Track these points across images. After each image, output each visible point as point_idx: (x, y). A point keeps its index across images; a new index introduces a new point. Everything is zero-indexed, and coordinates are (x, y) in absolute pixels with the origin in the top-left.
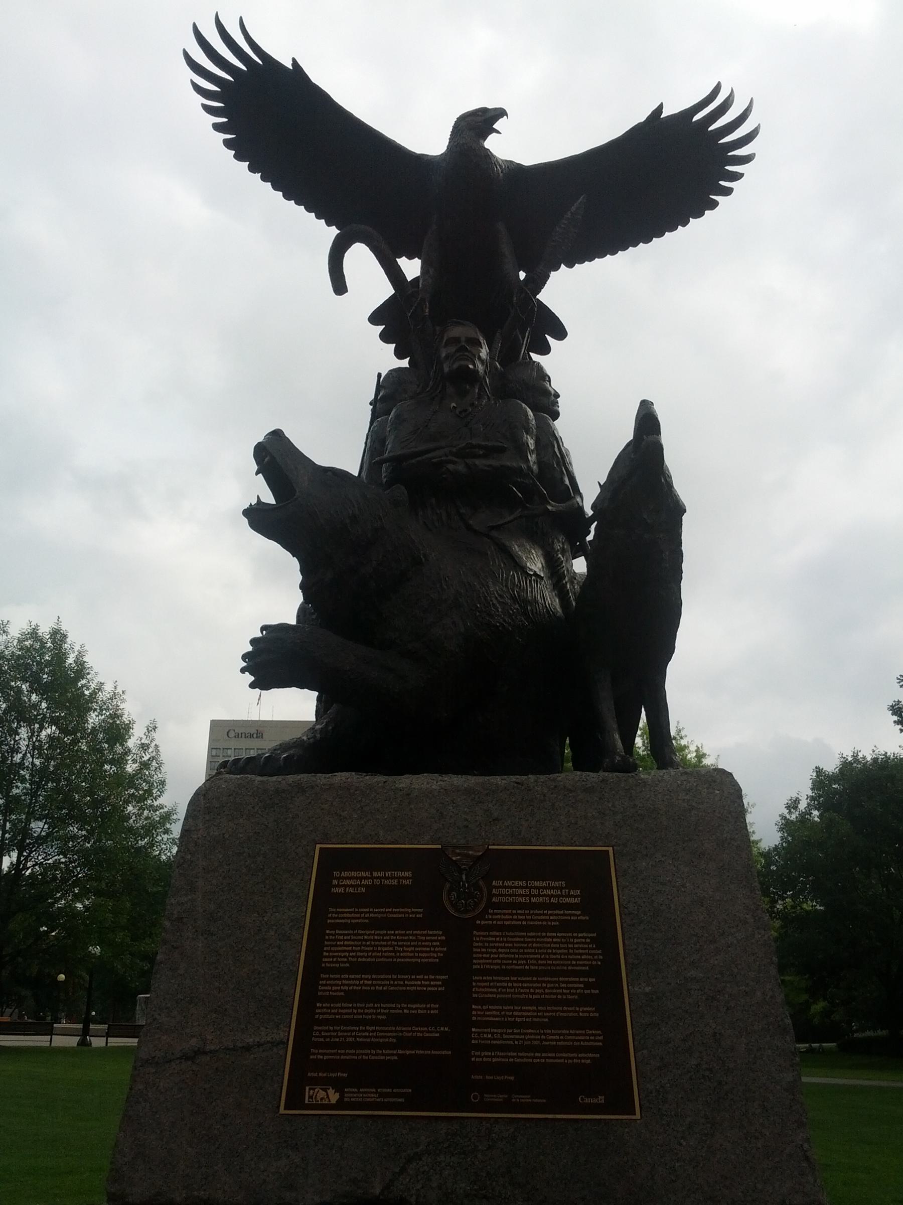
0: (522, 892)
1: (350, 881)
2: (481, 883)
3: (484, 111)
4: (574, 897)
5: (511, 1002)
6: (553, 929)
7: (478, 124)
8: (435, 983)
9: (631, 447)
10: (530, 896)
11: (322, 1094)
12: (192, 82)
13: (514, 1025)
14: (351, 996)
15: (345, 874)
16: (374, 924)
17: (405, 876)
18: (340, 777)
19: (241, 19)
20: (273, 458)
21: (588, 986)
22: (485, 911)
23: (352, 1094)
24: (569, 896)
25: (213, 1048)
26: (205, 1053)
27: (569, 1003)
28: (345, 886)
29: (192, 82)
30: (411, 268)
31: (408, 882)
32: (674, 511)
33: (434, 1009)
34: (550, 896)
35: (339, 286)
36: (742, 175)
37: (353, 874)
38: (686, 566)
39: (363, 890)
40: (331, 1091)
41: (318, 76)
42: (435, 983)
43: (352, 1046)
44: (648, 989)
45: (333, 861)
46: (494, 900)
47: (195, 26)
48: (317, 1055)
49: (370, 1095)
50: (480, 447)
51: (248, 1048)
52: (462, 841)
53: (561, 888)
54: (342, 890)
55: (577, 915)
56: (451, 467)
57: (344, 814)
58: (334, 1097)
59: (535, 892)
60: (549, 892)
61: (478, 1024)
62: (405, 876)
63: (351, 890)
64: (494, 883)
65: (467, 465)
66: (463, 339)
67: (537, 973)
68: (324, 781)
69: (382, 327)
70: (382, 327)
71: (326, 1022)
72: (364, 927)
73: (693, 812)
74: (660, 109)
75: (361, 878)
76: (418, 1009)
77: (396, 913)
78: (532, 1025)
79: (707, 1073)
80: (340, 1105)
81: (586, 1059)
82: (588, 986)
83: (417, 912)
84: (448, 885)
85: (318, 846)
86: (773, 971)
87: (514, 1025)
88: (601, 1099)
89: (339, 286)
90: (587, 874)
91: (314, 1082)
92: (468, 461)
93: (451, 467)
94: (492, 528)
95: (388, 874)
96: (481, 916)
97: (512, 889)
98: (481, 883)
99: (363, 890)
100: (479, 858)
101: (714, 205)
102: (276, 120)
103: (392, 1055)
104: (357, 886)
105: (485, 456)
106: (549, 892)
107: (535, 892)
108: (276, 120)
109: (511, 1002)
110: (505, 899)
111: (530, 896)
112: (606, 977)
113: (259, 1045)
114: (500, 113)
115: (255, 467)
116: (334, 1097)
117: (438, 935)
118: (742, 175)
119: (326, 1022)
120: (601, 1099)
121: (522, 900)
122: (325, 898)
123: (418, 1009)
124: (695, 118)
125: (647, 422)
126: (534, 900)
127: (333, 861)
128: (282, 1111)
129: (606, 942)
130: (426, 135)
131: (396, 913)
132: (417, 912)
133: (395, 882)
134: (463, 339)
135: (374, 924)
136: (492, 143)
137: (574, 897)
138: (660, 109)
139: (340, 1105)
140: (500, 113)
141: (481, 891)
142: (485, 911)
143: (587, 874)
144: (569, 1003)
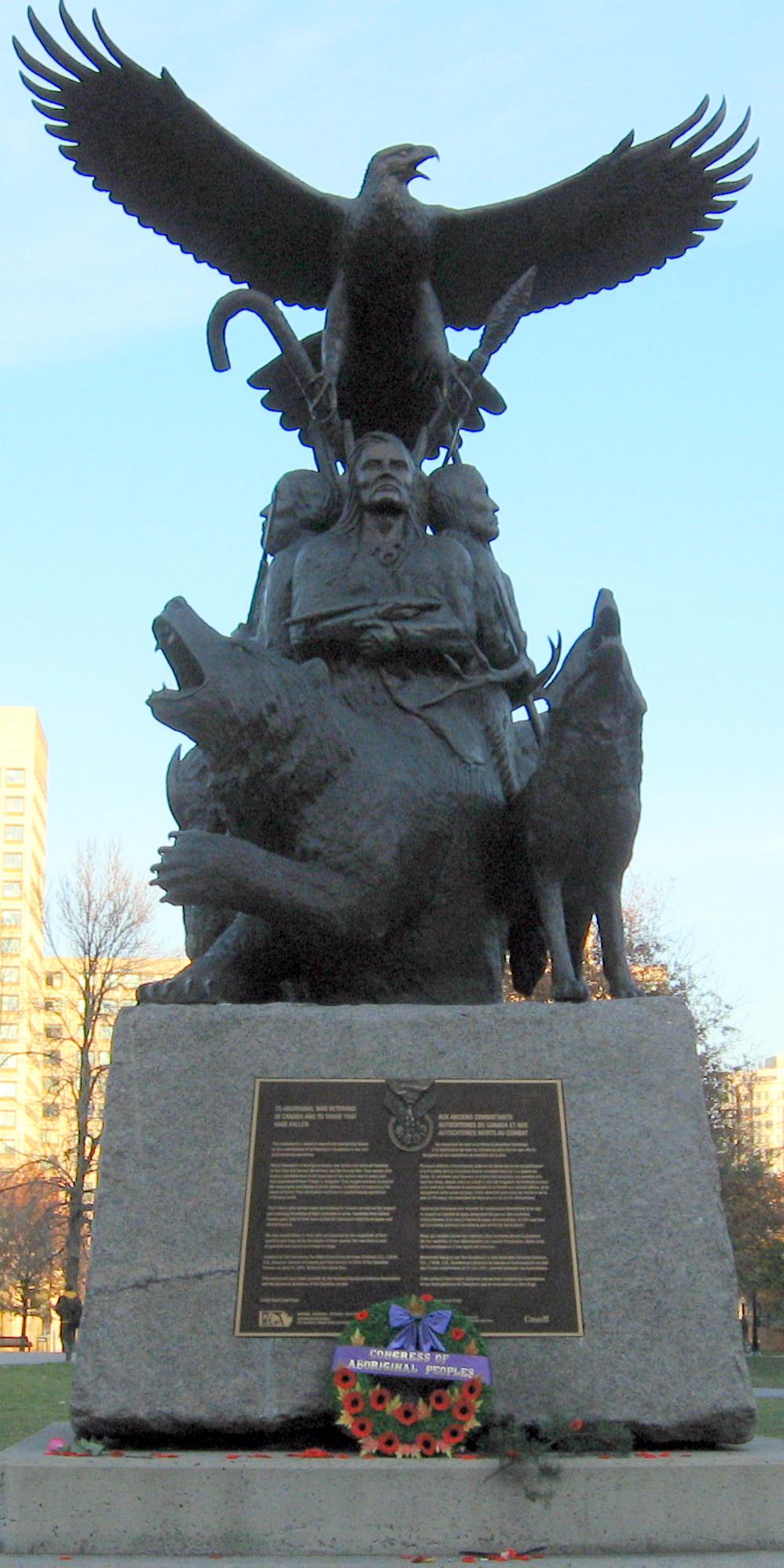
0: (469, 1125)
1: (293, 1116)
2: (427, 1117)
3: (410, 149)
4: (522, 1129)
5: (459, 1231)
6: (502, 1161)
7: (402, 164)
8: (382, 1214)
9: (587, 640)
10: (477, 1129)
11: (275, 1318)
12: (34, 102)
13: (458, 1252)
14: (300, 1227)
15: (287, 1108)
16: (319, 1158)
17: (350, 1111)
18: (276, 1009)
19: (94, 12)
20: (178, 639)
21: (534, 1214)
22: (432, 1144)
23: (305, 1318)
24: (517, 1129)
25: (164, 1276)
26: (157, 1281)
27: (515, 1231)
28: (289, 1121)
29: (34, 102)
30: (306, 322)
31: (353, 1117)
32: (634, 711)
33: (382, 1238)
34: (497, 1130)
35: (220, 361)
36: (734, 203)
37: (297, 1108)
38: (646, 767)
39: (307, 1124)
40: (284, 1315)
41: (196, 90)
42: (382, 1214)
43: (304, 1273)
44: (593, 1218)
45: (275, 1096)
46: (441, 1133)
47: (30, 10)
48: (268, 1282)
49: (322, 1318)
50: (409, 606)
51: (200, 1277)
52: (407, 1076)
53: (508, 1122)
54: (284, 1125)
55: (523, 1147)
56: (376, 633)
57: (283, 1047)
58: (287, 1321)
59: (481, 1125)
60: (495, 1125)
61: (426, 1252)
62: (350, 1111)
63: (295, 1125)
64: (441, 1117)
65: (396, 631)
66: (387, 462)
67: (487, 1203)
68: (259, 1013)
69: (265, 392)
70: (265, 392)
71: (274, 1251)
72: (308, 1160)
73: (645, 1044)
74: (630, 137)
75: (304, 1113)
76: (367, 1238)
77: (343, 1147)
78: (480, 1252)
79: (648, 1294)
80: (294, 1327)
81: (532, 1282)
82: (534, 1214)
83: (363, 1146)
84: (393, 1120)
85: (258, 1081)
86: (716, 1199)
87: (458, 1252)
88: (546, 1319)
89: (220, 361)
90: (537, 1107)
91: (268, 1307)
92: (396, 624)
93: (376, 633)
94: (425, 707)
95: (332, 1108)
96: (428, 1149)
97: (455, 1123)
98: (427, 1117)
99: (307, 1124)
100: (424, 1093)
101: (696, 242)
102: (134, 136)
103: (343, 1282)
104: (300, 1120)
105: (415, 617)
106: (495, 1125)
107: (481, 1125)
108: (134, 136)
109: (459, 1231)
110: (451, 1133)
111: (477, 1129)
112: (552, 1209)
113: (210, 1274)
114: (431, 154)
115: (154, 643)
116: (287, 1321)
117: (383, 1168)
118: (734, 203)
119: (274, 1251)
120: (546, 1319)
121: (469, 1133)
122: (267, 1133)
123: (367, 1238)
124: (674, 145)
125: (607, 617)
126: (481, 1133)
127: (275, 1096)
128: (238, 1333)
129: (553, 1174)
130: (334, 174)
131: (343, 1147)
132: (363, 1146)
133: (339, 1117)
134: (387, 462)
135: (319, 1158)
136: (416, 189)
137: (522, 1129)
138: (630, 137)
139: (294, 1327)
140: (431, 154)
141: (427, 1124)
142: (432, 1144)
143: (537, 1107)
144: (515, 1231)
